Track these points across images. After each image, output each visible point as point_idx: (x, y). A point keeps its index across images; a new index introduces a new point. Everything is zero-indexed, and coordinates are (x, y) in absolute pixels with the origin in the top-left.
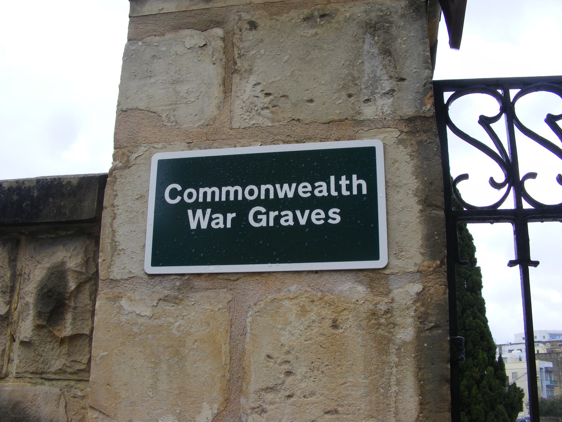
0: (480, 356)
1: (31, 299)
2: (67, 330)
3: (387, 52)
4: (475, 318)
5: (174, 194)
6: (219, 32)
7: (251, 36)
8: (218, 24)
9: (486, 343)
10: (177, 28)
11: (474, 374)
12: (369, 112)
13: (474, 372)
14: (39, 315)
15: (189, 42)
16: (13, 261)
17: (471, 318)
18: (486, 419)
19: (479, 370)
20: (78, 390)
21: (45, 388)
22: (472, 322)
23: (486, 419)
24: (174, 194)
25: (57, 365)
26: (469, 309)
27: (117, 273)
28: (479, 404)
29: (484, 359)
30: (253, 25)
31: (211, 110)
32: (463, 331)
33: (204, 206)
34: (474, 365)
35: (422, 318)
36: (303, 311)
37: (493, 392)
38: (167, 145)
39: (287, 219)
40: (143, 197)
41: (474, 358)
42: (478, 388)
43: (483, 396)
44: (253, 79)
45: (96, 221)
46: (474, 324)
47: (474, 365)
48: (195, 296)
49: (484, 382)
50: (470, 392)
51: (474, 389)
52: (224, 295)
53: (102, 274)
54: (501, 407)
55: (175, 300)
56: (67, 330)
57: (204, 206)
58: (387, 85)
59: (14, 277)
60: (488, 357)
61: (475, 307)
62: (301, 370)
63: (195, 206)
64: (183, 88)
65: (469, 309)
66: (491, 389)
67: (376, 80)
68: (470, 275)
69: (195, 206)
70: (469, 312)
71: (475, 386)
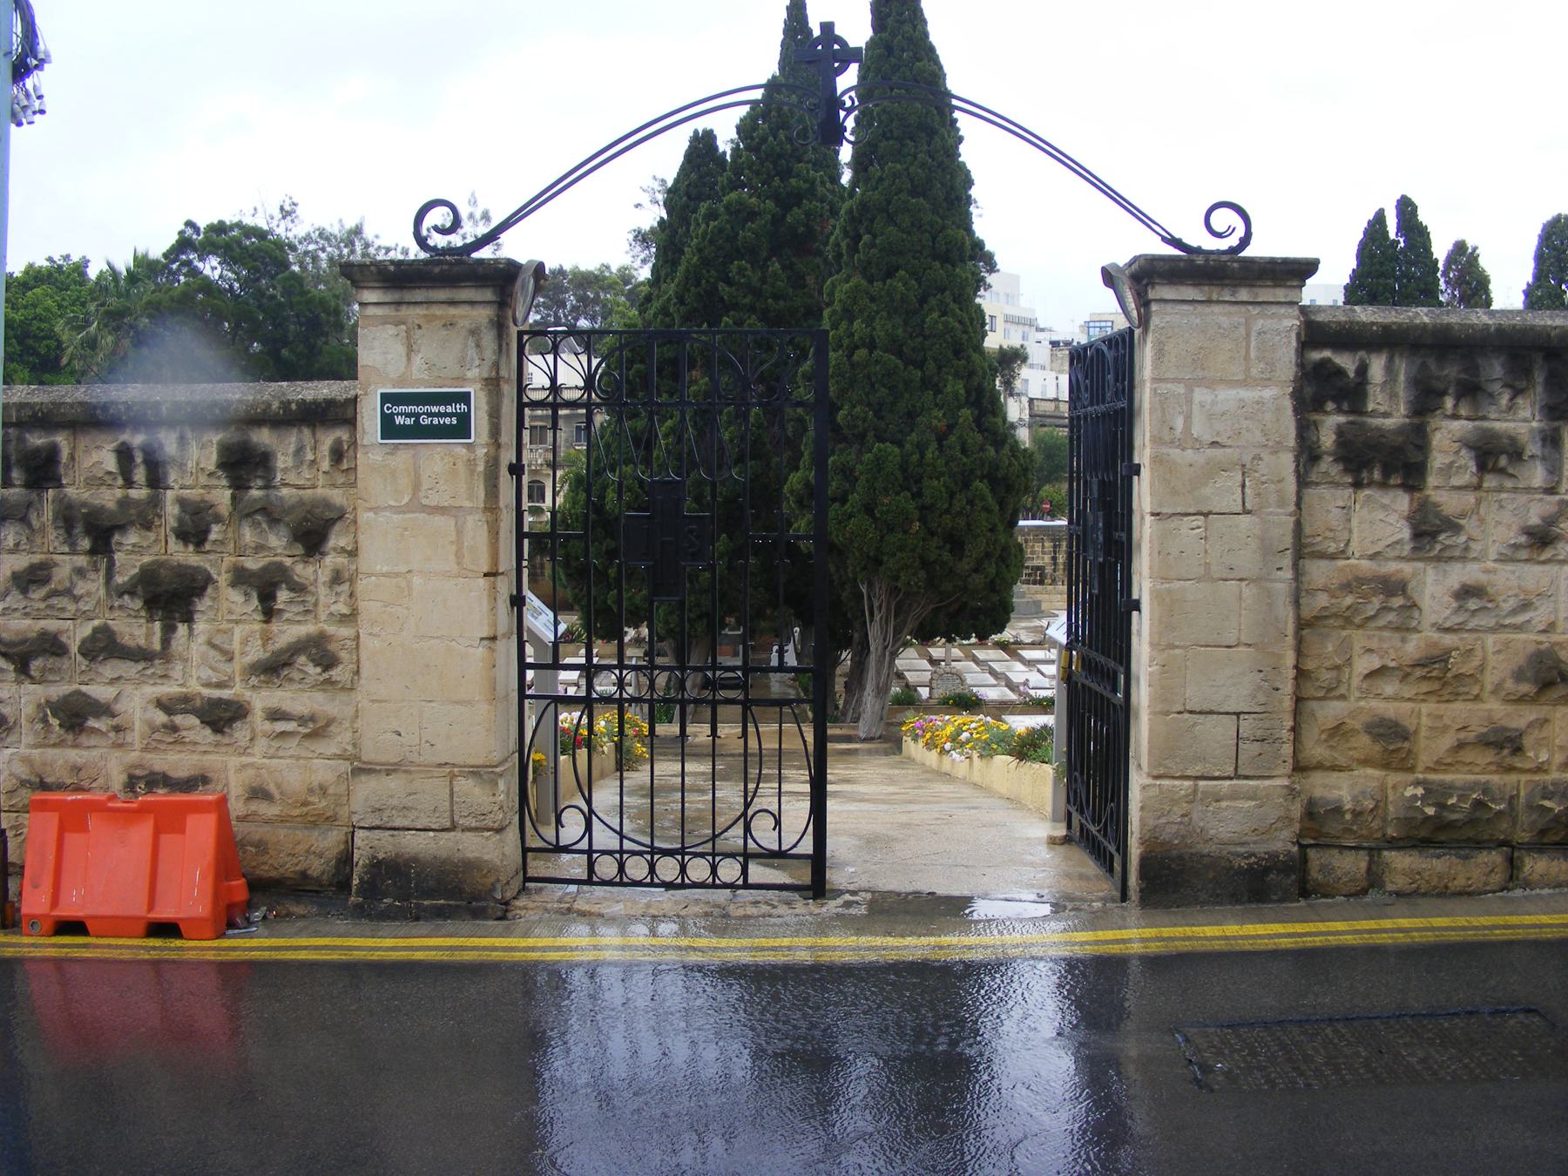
0: (949, 389)
1: (327, 453)
2: (345, 466)
3: (478, 346)
4: (944, 314)
5: (388, 408)
6: (403, 327)
7: (419, 332)
8: (404, 323)
9: (963, 362)
10: (385, 323)
11: (935, 422)
12: (469, 375)
13: (936, 417)
14: (332, 460)
15: (391, 332)
16: (314, 434)
17: (935, 315)
18: (950, 505)
19: (944, 415)
20: (352, 491)
21: (336, 491)
22: (937, 322)
23: (950, 505)
24: (388, 408)
25: (341, 481)
26: (935, 296)
27: (365, 442)
28: (938, 478)
29: (956, 394)
30: (420, 327)
31: (402, 369)
32: (920, 339)
33: (402, 414)
34: (936, 405)
35: (487, 462)
36: (442, 459)
37: (967, 456)
38: (384, 386)
39: (436, 421)
40: (375, 409)
41: (938, 391)
42: (940, 448)
43: (947, 464)
44: (420, 355)
45: (355, 418)
46: (940, 326)
47: (936, 405)
48: (399, 452)
49: (952, 438)
50: (922, 456)
51: (931, 449)
52: (412, 452)
53: (359, 442)
54: (981, 486)
55: (392, 454)
56: (345, 466)
57: (402, 414)
58: (477, 362)
59: (316, 442)
60: (967, 392)
61: (947, 293)
62: (441, 482)
63: (398, 414)
64: (390, 357)
65: (935, 296)
66: (964, 451)
67: (473, 359)
68: (944, 228)
69: (398, 414)
70: (933, 301)
71: (934, 445)
